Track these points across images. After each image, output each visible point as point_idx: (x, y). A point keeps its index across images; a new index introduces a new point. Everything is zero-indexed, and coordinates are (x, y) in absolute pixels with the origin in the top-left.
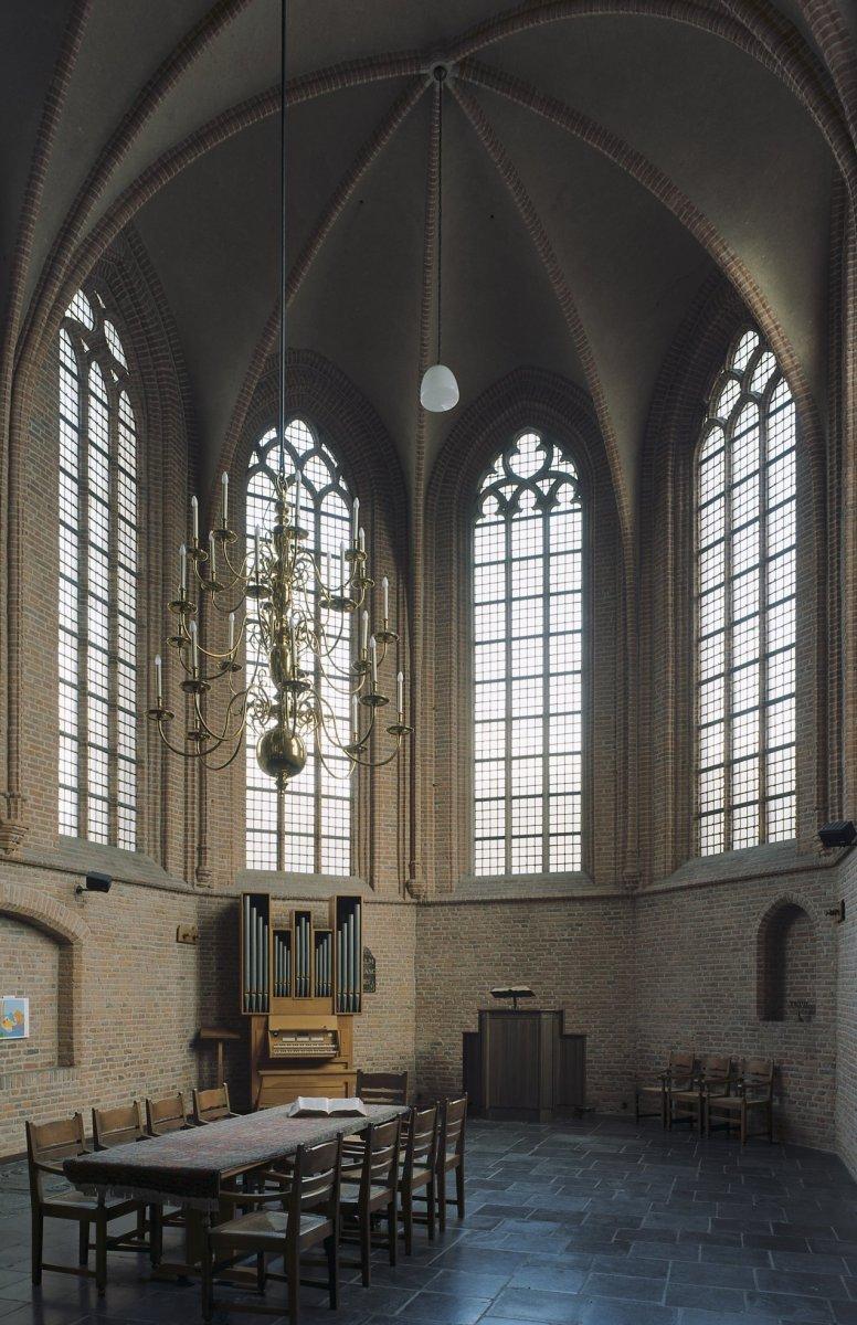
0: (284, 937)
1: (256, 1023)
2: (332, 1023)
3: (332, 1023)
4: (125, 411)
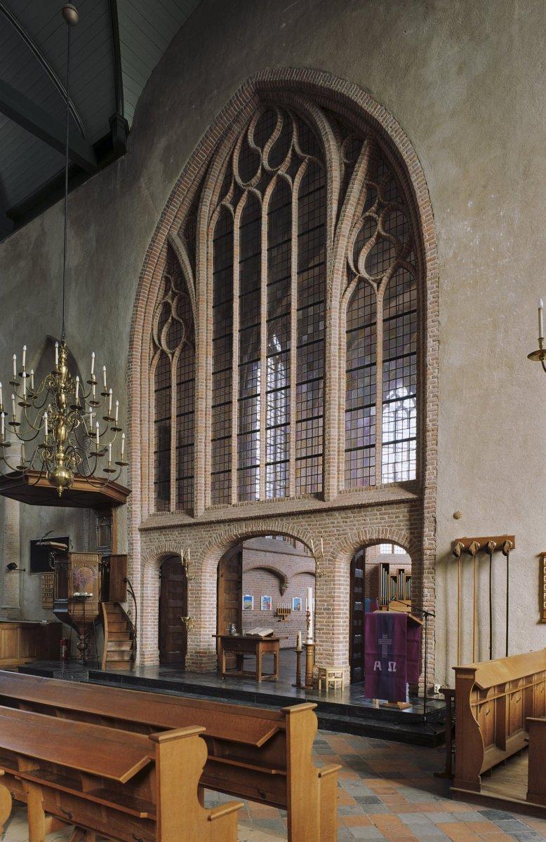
4: (258, 115)
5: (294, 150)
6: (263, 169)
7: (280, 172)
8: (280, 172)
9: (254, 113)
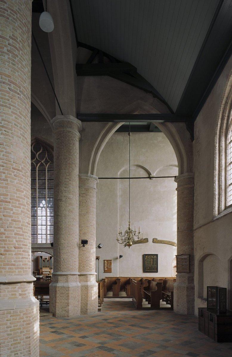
0: (44, 261)
1: (41, 270)
2: (49, 270)
3: (49, 270)
5: (46, 158)
6: (37, 159)
7: (42, 162)
8: (42, 162)
9: (34, 143)
